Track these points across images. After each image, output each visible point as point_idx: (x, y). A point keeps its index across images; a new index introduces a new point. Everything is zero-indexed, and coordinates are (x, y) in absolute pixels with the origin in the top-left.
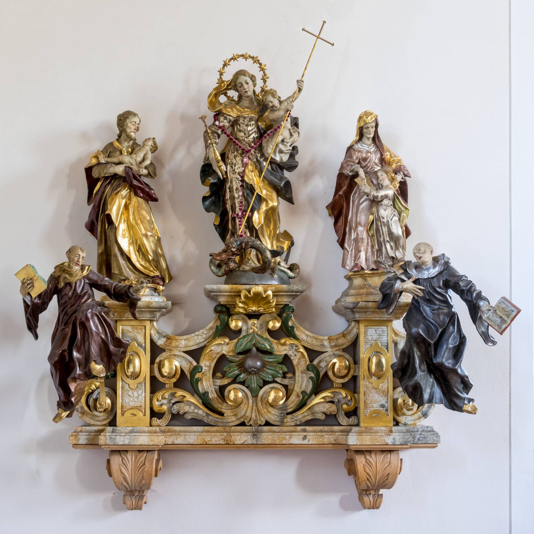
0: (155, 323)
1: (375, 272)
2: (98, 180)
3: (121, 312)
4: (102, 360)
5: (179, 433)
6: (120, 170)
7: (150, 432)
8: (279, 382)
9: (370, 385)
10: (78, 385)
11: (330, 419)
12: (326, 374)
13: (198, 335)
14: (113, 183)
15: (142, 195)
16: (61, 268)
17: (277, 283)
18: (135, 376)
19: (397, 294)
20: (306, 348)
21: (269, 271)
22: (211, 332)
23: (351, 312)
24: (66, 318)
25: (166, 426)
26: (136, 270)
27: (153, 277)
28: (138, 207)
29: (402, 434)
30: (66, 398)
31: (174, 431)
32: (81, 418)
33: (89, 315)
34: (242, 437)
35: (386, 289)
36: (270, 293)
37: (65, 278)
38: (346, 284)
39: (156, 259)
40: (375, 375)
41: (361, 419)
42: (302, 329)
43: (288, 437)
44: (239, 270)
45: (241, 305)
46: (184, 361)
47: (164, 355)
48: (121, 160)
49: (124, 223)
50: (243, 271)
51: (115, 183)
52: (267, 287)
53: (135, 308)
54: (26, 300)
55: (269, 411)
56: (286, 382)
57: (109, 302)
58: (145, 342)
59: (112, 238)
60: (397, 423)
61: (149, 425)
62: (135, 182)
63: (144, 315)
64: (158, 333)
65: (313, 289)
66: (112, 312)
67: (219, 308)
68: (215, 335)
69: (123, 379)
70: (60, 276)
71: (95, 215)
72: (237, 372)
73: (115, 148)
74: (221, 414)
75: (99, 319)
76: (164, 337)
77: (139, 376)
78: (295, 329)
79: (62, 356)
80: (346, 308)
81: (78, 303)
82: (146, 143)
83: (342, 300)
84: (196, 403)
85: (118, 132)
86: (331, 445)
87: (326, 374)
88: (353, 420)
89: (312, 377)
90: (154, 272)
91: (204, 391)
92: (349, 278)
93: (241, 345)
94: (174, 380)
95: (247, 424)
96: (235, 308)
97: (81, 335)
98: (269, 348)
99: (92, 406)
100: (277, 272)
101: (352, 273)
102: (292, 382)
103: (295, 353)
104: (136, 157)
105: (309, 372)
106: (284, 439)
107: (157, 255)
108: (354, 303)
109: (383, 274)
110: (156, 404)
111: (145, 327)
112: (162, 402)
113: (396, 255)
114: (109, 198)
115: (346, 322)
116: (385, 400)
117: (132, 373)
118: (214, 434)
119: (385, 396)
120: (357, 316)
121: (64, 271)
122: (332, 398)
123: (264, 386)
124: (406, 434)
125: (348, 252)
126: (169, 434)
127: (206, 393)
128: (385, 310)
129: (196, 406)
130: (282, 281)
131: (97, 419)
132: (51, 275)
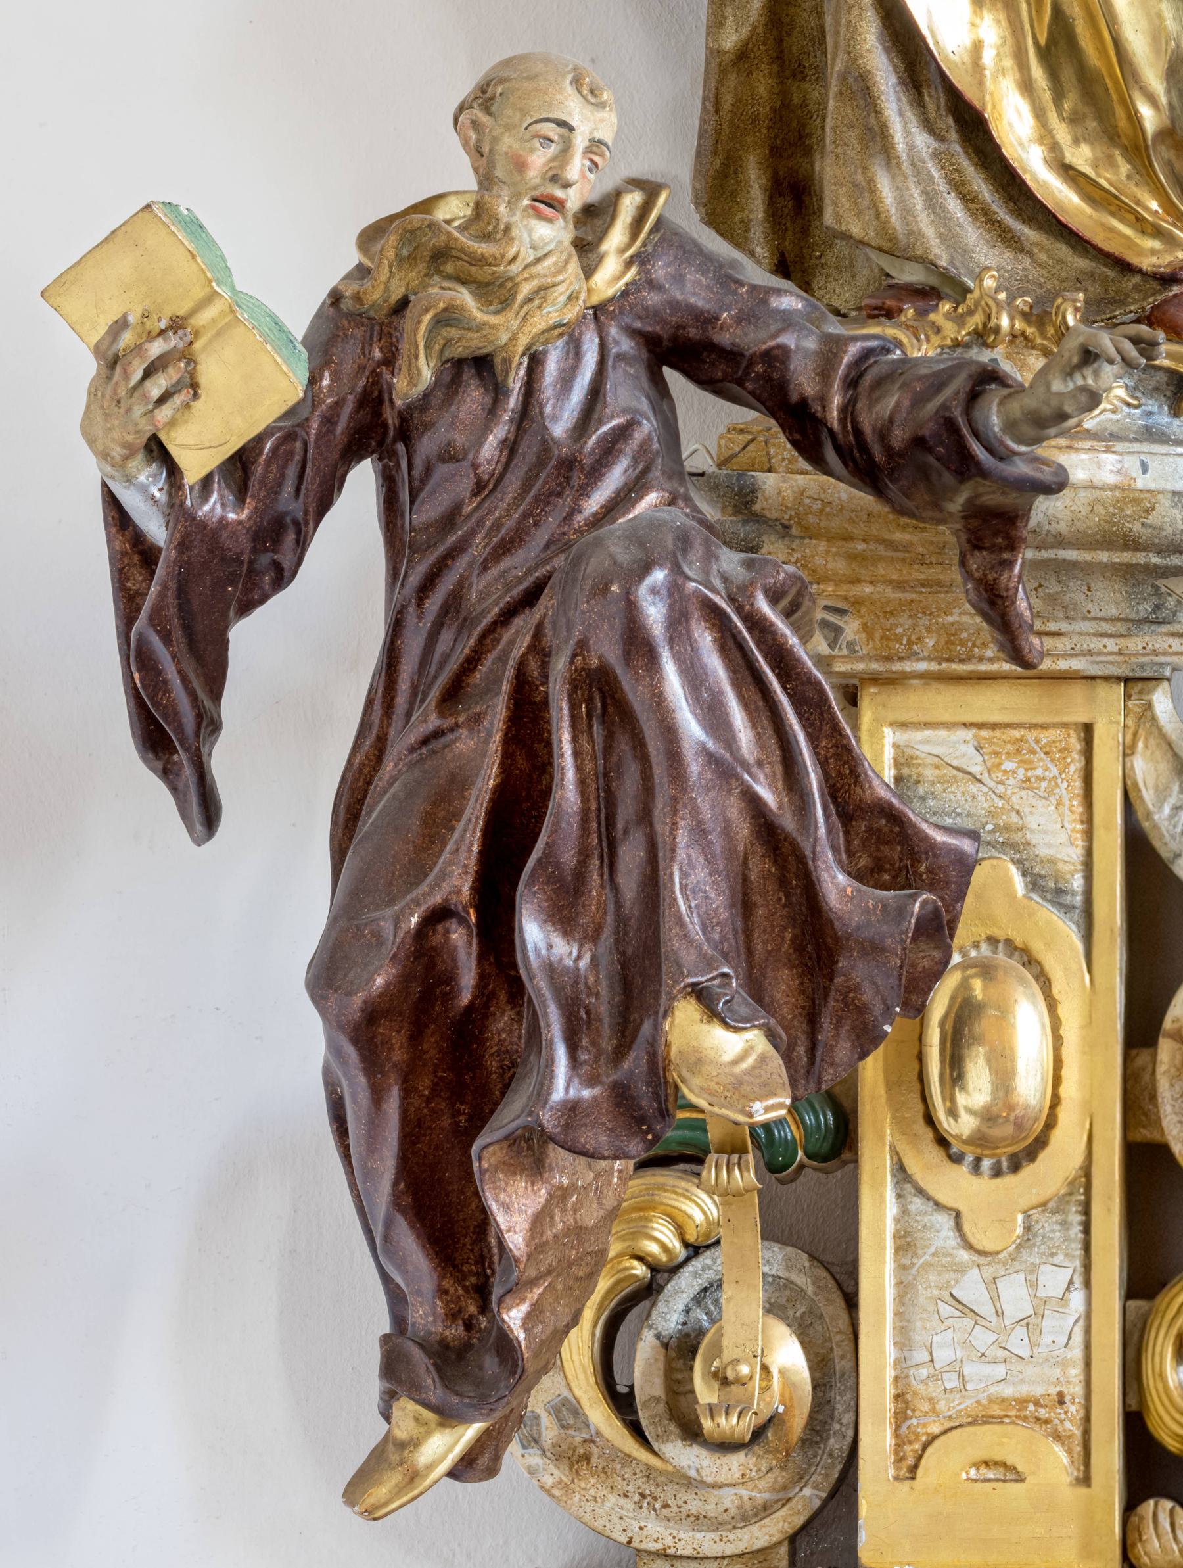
4: (757, 990)
10: (560, 1196)
16: (410, 236)
18: (1017, 1146)
24: (454, 647)
26: (1018, 213)
30: (453, 1315)
32: (557, 1495)
33: (654, 613)
37: (448, 318)
53: (1012, 545)
54: (131, 500)
57: (786, 481)
69: (913, 1166)
70: (404, 303)
75: (730, 644)
77: (1041, 1142)
79: (425, 960)
81: (551, 524)
90: (1169, 240)
97: (582, 783)
99: (659, 1404)
117: (988, 1116)
121: (440, 258)
131: (694, 1506)
132: (335, 297)
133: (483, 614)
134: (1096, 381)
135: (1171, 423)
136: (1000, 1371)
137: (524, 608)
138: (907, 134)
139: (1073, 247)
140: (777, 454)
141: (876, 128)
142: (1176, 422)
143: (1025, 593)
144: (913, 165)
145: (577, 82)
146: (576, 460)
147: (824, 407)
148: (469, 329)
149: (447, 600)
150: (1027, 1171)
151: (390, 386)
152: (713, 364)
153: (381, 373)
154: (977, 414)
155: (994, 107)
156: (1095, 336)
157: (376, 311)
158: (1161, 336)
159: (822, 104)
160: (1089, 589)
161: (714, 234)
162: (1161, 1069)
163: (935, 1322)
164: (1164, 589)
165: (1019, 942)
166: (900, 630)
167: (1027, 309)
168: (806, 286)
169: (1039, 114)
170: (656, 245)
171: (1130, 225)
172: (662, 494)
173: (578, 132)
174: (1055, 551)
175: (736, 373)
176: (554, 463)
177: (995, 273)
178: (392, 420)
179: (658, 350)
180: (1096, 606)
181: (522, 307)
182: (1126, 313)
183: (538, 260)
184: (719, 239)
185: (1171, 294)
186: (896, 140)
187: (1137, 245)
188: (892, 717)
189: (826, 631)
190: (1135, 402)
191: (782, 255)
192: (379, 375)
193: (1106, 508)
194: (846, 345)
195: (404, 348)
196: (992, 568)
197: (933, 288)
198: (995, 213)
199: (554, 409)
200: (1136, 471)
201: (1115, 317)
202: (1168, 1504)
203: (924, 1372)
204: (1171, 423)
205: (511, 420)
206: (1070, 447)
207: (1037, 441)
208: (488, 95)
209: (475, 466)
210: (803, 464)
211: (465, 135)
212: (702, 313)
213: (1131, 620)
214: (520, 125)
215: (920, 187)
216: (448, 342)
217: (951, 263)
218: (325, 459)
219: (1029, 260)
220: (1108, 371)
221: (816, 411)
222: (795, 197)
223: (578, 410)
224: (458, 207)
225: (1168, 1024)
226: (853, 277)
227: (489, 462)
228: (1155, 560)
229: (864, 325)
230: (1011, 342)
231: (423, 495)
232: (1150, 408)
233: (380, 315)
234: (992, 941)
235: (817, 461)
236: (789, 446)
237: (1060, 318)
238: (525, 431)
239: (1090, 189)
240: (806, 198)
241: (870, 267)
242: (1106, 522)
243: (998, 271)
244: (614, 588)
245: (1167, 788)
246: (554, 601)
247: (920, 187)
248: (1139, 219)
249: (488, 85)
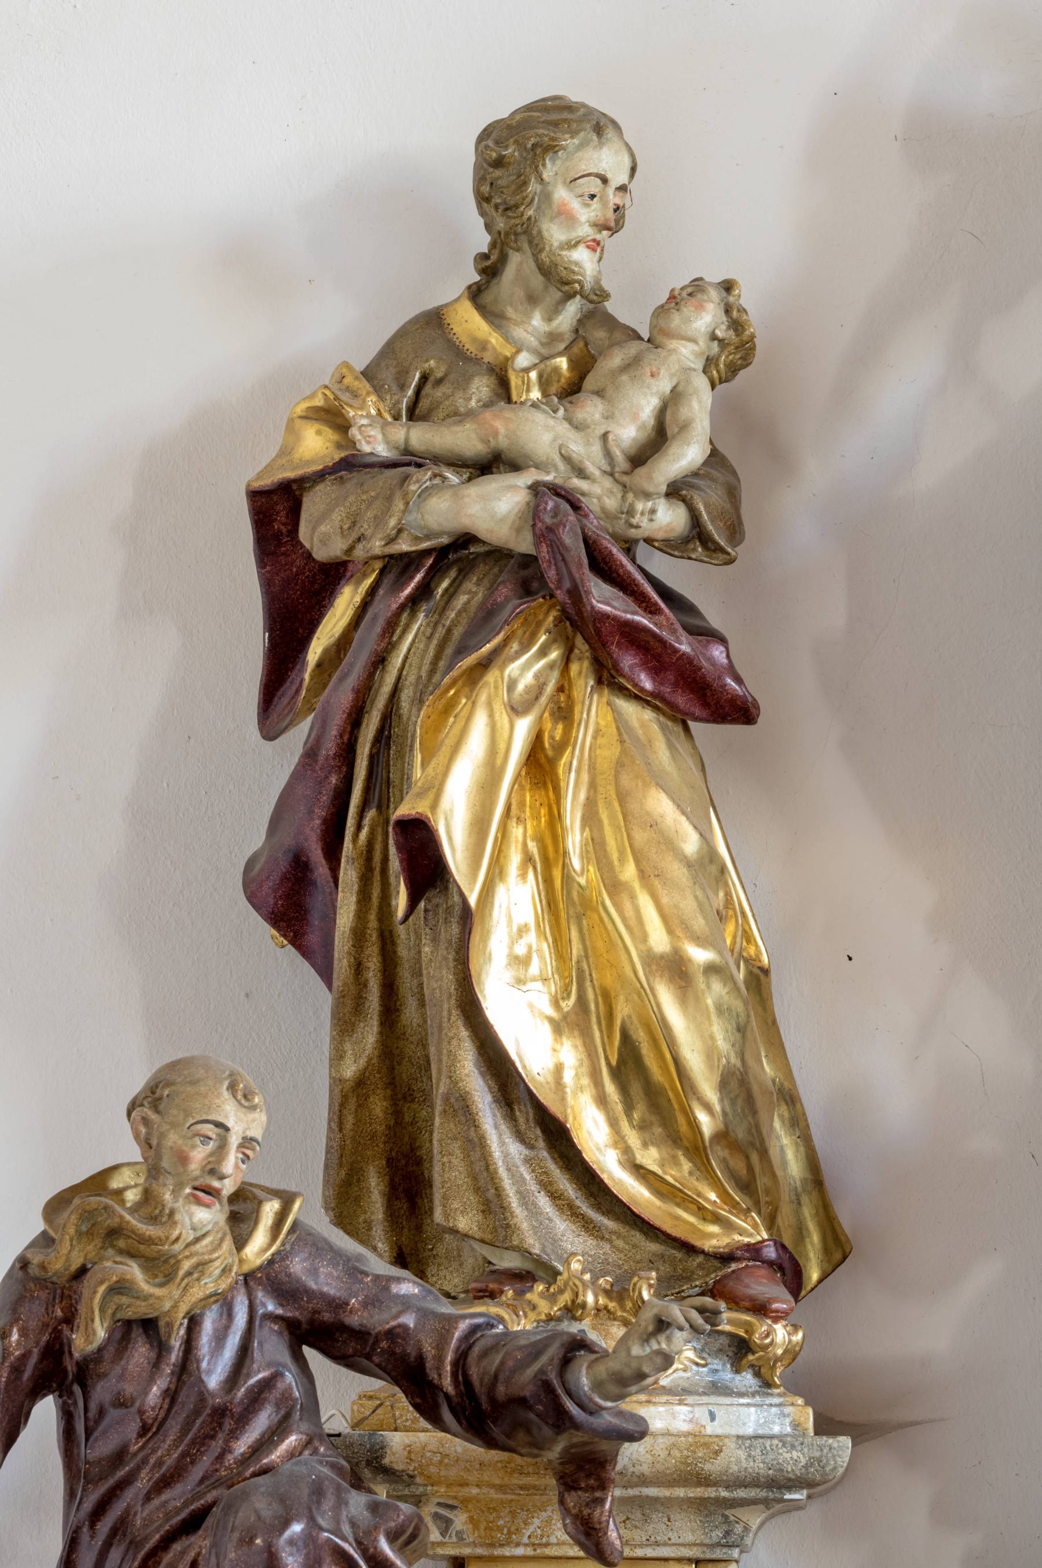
2: (333, 575)
3: (493, 1509)
6: (495, 509)
14: (450, 594)
15: (648, 685)
16: (88, 1215)
26: (598, 1207)
27: (726, 1258)
28: (620, 765)
37: (121, 1288)
39: (740, 1133)
48: (502, 442)
49: (523, 876)
51: (462, 599)
53: (603, 1485)
57: (410, 1438)
59: (440, 981)
62: (603, 599)
63: (657, 1527)
70: (83, 1271)
71: (321, 812)
73: (458, 352)
81: (206, 1461)
82: (676, 321)
85: (482, 241)
90: (728, 1226)
104: (608, 417)
114: (419, 701)
132: (23, 1263)
133: (146, 1539)
134: (668, 1346)
135: (733, 1379)
137: (181, 1535)
138: (502, 1144)
139: (646, 1234)
140: (401, 1416)
141: (476, 1140)
142: (738, 1377)
143: (615, 1525)
144: (509, 1170)
145: (232, 1088)
146: (227, 1408)
147: (440, 1375)
148: (138, 1298)
149: (116, 1523)
151: (70, 1342)
152: (345, 1342)
153: (62, 1330)
154: (570, 1377)
155: (575, 1118)
156: (667, 1307)
157: (58, 1277)
158: (722, 1305)
159: (430, 1119)
160: (669, 1520)
161: (341, 1233)
164: (732, 1518)
166: (501, 1522)
167: (608, 1287)
168: (421, 1274)
169: (613, 1123)
170: (293, 1244)
171: (692, 1214)
172: (300, 1436)
173: (233, 1131)
174: (639, 1489)
175: (365, 1349)
176: (208, 1411)
177: (580, 1258)
178: (71, 1368)
179: (298, 1332)
180: (675, 1534)
181: (183, 1279)
182: (692, 1288)
183: (197, 1240)
184: (346, 1237)
185: (729, 1270)
186: (493, 1149)
187: (699, 1230)
189: (438, 1522)
190: (703, 1362)
191: (400, 1248)
192: (60, 1332)
193: (681, 1451)
194: (457, 1322)
195: (82, 1309)
196: (587, 1505)
197: (528, 1272)
198: (579, 1207)
199: (209, 1364)
200: (705, 1419)
201: (683, 1291)
204: (733, 1379)
205: (172, 1373)
206: (649, 1402)
207: (621, 1397)
208: (157, 1095)
209: (141, 1412)
210: (423, 1423)
211: (137, 1129)
212: (334, 1300)
213: (706, 1545)
214: (184, 1124)
215: (515, 1188)
216: (119, 1308)
217: (543, 1250)
218: (13, 1401)
219: (609, 1246)
220: (679, 1336)
221: (433, 1379)
222: (409, 1187)
223: (230, 1363)
224: (130, 1177)
226: (461, 1265)
227: (153, 1409)
228: (724, 1493)
229: (471, 1304)
230: (596, 1315)
231: (96, 1434)
232: (715, 1367)
233: (62, 1281)
235: (436, 1420)
236: (411, 1408)
237: (637, 1293)
238: (184, 1383)
239: (658, 1184)
240: (419, 1201)
241: (475, 1257)
242: (682, 1463)
243: (583, 1256)
244: (258, 1541)
246: (207, 1542)
247: (515, 1188)
248: (701, 1208)
249: (157, 1087)
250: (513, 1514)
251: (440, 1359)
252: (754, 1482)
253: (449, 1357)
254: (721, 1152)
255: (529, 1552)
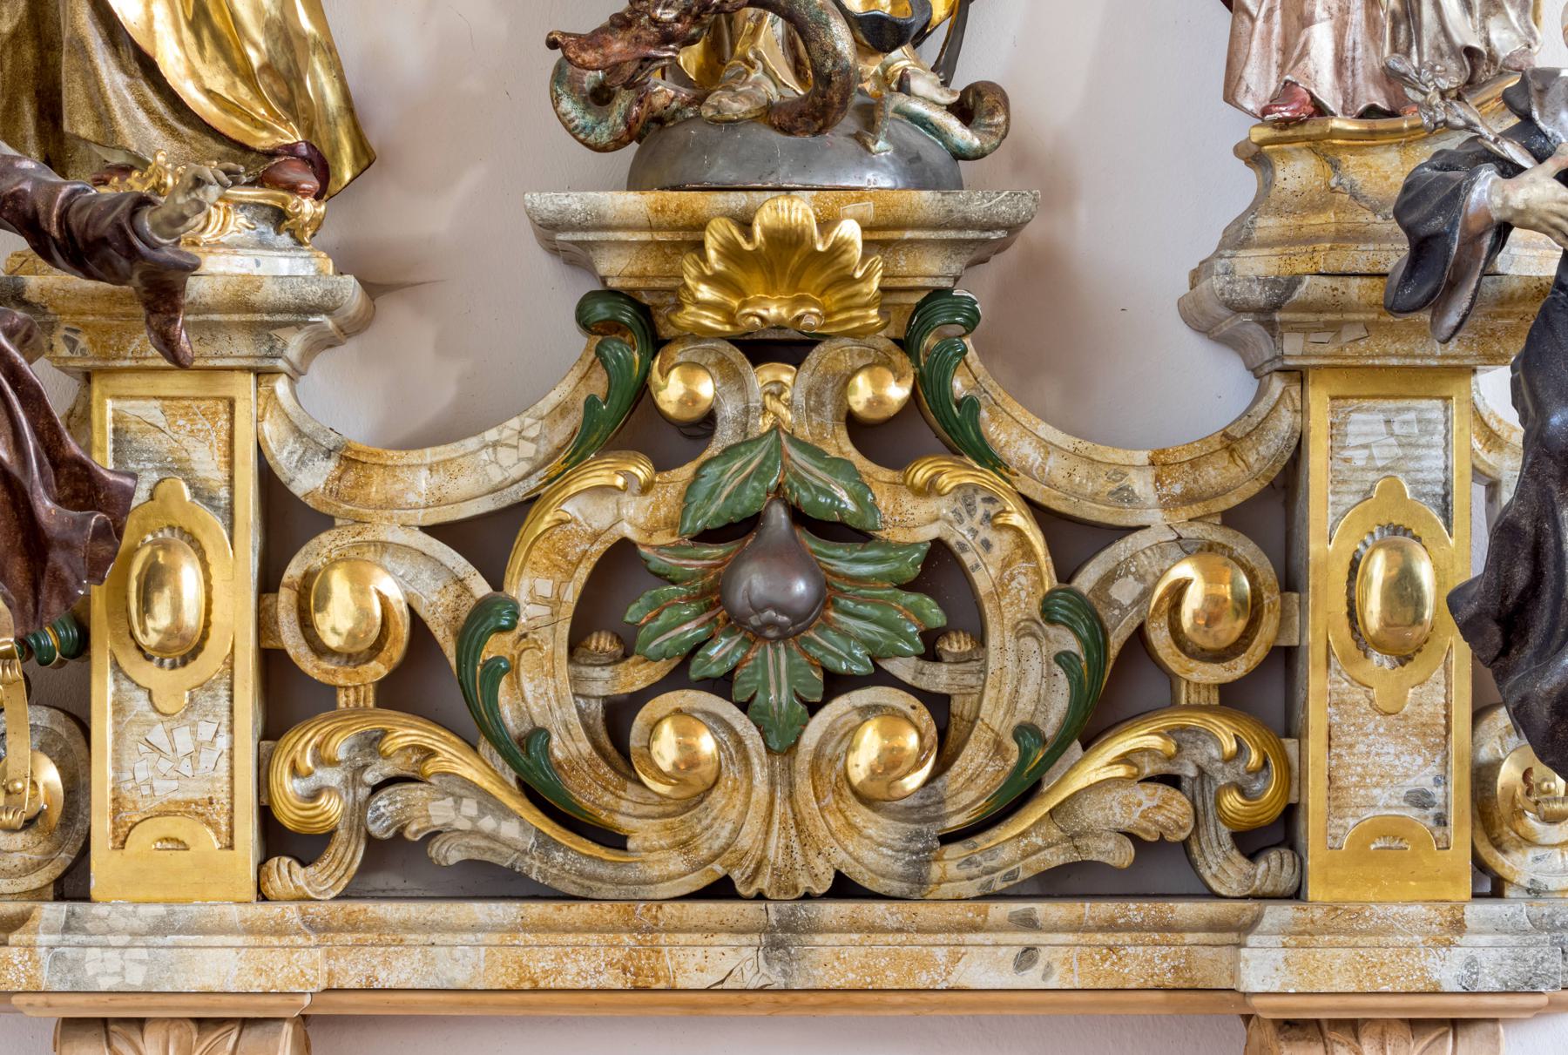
0: (281, 386)
1: (1381, 124)
3: (106, 331)
5: (391, 936)
7: (250, 930)
8: (908, 678)
9: (1359, 695)
11: (1160, 865)
12: (1139, 636)
13: (495, 445)
17: (888, 183)
18: (185, 649)
19: (1481, 235)
20: (1037, 510)
21: (849, 123)
22: (562, 432)
23: (1261, 323)
25: (337, 898)
26: (181, 120)
27: (271, 154)
29: (1513, 940)
31: (378, 926)
34: (713, 955)
35: (1427, 208)
36: (849, 230)
38: (1247, 181)
39: (282, 65)
40: (1380, 646)
41: (1310, 863)
42: (1018, 411)
43: (940, 954)
44: (698, 116)
45: (705, 292)
46: (425, 576)
47: (323, 547)
50: (714, 122)
52: (839, 200)
53: (176, 309)
55: (851, 826)
56: (939, 678)
58: (232, 477)
60: (1491, 885)
61: (250, 891)
63: (222, 344)
64: (298, 432)
65: (1082, 213)
66: (61, 332)
67: (601, 311)
68: (581, 442)
72: (691, 630)
74: (614, 840)
76: (328, 454)
78: (984, 414)
80: (1237, 308)
83: (1219, 266)
84: (486, 784)
86: (1160, 996)
87: (1139, 636)
88: (1272, 869)
89: (1067, 654)
91: (527, 727)
92: (1256, 157)
93: (711, 495)
94: (378, 669)
95: (741, 890)
96: (679, 306)
98: (852, 507)
100: (886, 126)
101: (1267, 132)
102: (971, 680)
103: (986, 533)
105: (1052, 631)
106: (925, 963)
107: (288, 42)
108: (1275, 281)
109: (1419, 134)
110: (288, 788)
111: (231, 404)
112: (315, 782)
113: (1488, 42)
115: (1249, 376)
116: (1434, 769)
117: (175, 631)
118: (570, 938)
119: (1432, 748)
120: (1293, 346)
122: (1169, 758)
123: (829, 696)
124: (1529, 939)
125: (1253, 19)
126: (349, 938)
127: (537, 736)
128: (1425, 316)
129: (487, 801)
130: (917, 173)
136: (175, 784)
150: (191, 666)
154: (137, 222)
162: (281, 606)
163: (136, 755)
165: (186, 528)
188: (110, 392)
202: (287, 860)
203: (130, 785)
225: (285, 579)
228: (266, 318)
234: (171, 528)
245: (286, 441)
248: (253, 119)
250: (120, 336)
251: (49, 213)
252: (285, 309)
253: (55, 212)
254: (267, 79)
255: (133, 363)
